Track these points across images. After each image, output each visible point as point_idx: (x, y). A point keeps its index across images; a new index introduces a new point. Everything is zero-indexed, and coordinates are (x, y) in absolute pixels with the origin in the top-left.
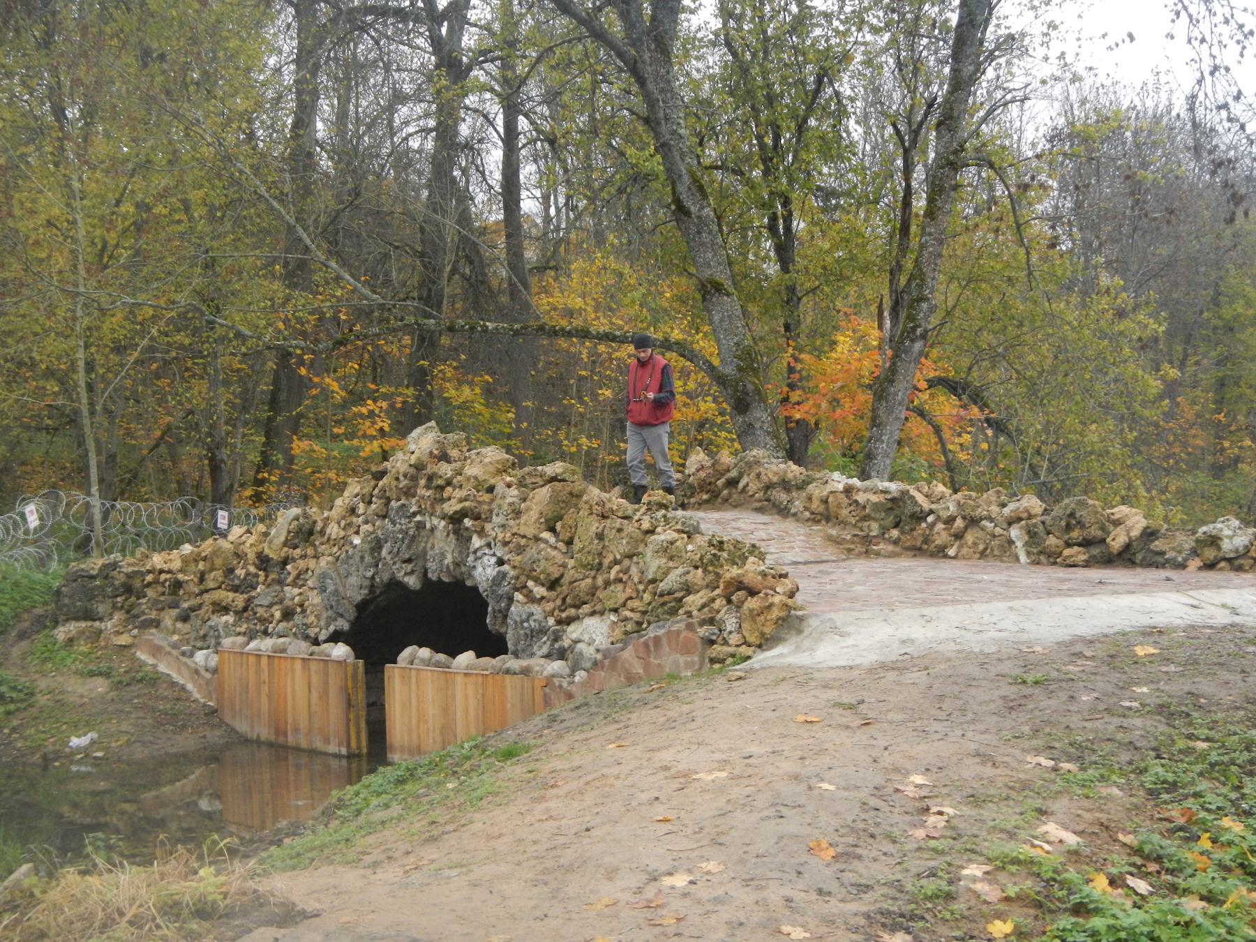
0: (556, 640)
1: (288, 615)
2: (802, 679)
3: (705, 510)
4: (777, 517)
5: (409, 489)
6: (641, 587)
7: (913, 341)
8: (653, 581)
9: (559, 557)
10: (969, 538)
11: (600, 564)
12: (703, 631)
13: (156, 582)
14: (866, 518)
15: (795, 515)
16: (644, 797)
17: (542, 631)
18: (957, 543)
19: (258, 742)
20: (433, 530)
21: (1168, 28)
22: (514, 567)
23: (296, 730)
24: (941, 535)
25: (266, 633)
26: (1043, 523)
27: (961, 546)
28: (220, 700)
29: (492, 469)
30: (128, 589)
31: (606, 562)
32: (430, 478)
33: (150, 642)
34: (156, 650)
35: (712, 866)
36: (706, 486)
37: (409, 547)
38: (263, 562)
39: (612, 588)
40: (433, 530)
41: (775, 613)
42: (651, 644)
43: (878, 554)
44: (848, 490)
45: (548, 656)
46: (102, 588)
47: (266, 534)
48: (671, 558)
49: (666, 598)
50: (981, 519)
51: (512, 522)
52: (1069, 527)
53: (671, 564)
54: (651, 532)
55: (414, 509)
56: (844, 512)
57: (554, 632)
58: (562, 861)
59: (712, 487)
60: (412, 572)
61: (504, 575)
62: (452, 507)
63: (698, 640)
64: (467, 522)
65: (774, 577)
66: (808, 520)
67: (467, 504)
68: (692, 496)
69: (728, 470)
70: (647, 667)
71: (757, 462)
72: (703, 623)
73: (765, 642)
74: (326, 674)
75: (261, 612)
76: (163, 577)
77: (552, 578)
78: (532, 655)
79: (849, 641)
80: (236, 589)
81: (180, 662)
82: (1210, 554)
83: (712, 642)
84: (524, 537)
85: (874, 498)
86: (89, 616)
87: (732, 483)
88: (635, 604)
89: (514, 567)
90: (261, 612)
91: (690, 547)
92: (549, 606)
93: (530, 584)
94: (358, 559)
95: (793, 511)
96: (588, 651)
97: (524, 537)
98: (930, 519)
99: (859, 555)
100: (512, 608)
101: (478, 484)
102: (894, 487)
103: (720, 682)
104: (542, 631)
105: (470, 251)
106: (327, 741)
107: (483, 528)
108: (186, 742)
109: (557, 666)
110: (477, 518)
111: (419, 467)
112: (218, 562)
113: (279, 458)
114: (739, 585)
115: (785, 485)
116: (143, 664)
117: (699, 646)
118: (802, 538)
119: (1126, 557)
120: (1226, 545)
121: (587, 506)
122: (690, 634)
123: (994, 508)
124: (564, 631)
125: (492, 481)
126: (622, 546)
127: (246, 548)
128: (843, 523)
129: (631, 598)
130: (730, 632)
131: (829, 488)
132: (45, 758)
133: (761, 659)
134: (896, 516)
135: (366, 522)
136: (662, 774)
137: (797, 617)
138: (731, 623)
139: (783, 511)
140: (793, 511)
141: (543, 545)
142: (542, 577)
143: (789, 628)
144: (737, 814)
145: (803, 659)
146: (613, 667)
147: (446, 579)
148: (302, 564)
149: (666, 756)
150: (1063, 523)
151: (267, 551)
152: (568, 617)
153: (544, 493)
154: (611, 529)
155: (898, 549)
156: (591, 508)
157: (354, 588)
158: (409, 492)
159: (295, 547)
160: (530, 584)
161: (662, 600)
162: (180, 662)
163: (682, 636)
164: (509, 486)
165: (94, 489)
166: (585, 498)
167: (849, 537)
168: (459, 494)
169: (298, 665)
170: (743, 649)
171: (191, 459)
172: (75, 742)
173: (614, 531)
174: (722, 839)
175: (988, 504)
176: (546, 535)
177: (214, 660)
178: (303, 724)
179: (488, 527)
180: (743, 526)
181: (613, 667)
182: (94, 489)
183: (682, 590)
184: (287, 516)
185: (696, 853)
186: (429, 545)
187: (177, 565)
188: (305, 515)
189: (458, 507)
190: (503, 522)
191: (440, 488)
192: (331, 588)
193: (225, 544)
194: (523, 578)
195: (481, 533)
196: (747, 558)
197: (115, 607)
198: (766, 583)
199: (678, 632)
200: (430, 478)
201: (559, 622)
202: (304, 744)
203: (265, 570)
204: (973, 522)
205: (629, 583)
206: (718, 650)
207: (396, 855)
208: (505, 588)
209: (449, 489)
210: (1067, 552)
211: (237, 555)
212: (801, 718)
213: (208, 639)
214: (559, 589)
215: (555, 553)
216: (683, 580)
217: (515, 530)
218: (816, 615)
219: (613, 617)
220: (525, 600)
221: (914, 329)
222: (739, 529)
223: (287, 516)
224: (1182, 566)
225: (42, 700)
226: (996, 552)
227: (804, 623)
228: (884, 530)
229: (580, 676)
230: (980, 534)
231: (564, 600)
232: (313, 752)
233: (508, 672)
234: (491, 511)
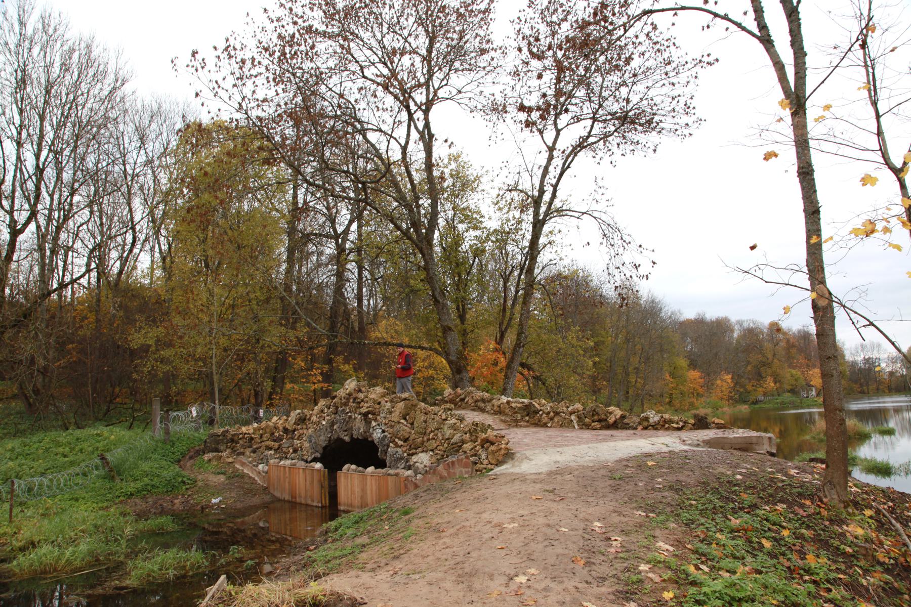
1: (295, 451)
2: (522, 478)
8: (448, 439)
10: (556, 420)
12: (472, 459)
13: (243, 438)
14: (516, 413)
16: (486, 536)
17: (402, 458)
19: (284, 501)
20: (355, 418)
21: (601, 240)
23: (300, 497)
24: (545, 418)
25: (286, 458)
28: (269, 484)
30: (232, 441)
31: (428, 432)
32: (355, 399)
33: (241, 461)
34: (243, 464)
35: (533, 571)
38: (286, 430)
40: (355, 418)
41: (503, 452)
43: (521, 426)
44: (508, 402)
45: (404, 468)
46: (222, 440)
47: (287, 420)
54: (446, 420)
58: (466, 571)
62: (364, 410)
64: (370, 416)
70: (449, 473)
72: (472, 456)
73: (499, 463)
74: (313, 474)
75: (284, 449)
78: (398, 468)
79: (533, 462)
80: (275, 441)
81: (253, 469)
82: (646, 424)
83: (476, 463)
85: (519, 405)
86: (217, 450)
87: (462, 400)
88: (441, 448)
90: (284, 449)
92: (405, 449)
96: (421, 466)
101: (375, 401)
102: (526, 401)
103: (486, 480)
104: (402, 458)
105: (347, 313)
106: (313, 501)
108: (256, 500)
109: (410, 472)
110: (374, 414)
111: (350, 394)
112: (268, 430)
113: (278, 390)
114: (486, 441)
115: (483, 400)
116: (238, 469)
119: (615, 426)
120: (651, 420)
123: (565, 408)
126: (435, 425)
127: (279, 425)
128: (507, 415)
131: (500, 402)
132: (202, 508)
133: (498, 470)
136: (489, 526)
138: (484, 456)
144: (532, 544)
145: (516, 470)
146: (434, 473)
148: (301, 431)
149: (486, 516)
157: (323, 441)
158: (346, 404)
162: (253, 469)
165: (217, 402)
169: (301, 471)
170: (489, 466)
171: (247, 389)
174: (533, 558)
175: (562, 407)
176: (402, 421)
177: (266, 468)
178: (303, 494)
181: (434, 473)
184: (294, 414)
185: (523, 565)
187: (251, 431)
188: (303, 413)
191: (359, 403)
193: (270, 424)
195: (376, 420)
197: (227, 447)
200: (355, 399)
202: (303, 502)
204: (557, 414)
206: (479, 466)
207: (382, 565)
211: (275, 428)
212: (534, 497)
213: (264, 460)
223: (294, 414)
224: (636, 429)
225: (200, 484)
228: (523, 417)
229: (419, 476)
232: (307, 505)
233: (389, 475)
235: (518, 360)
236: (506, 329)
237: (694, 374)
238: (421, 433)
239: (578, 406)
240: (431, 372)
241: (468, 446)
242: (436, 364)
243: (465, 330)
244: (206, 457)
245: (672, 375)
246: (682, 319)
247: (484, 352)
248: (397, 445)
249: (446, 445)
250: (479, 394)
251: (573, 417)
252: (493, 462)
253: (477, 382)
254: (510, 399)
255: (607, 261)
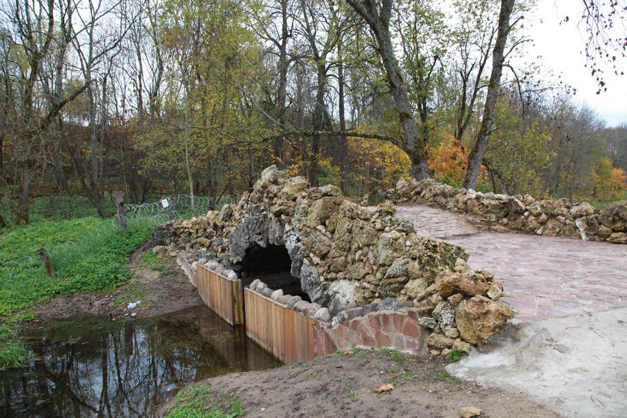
0: (325, 289)
3: (406, 206)
4: (440, 210)
5: (260, 198)
6: (375, 268)
7: (485, 136)
8: (383, 265)
9: (327, 241)
10: (550, 225)
11: (350, 248)
15: (449, 209)
17: (318, 284)
18: (542, 227)
22: (304, 244)
24: (532, 222)
26: (596, 218)
27: (544, 229)
29: (296, 188)
30: (175, 234)
31: (354, 247)
36: (405, 194)
37: (259, 227)
38: (215, 226)
39: (357, 265)
41: (492, 321)
42: (381, 319)
43: (496, 231)
44: (478, 198)
48: (395, 250)
49: (392, 280)
50: (558, 215)
51: (303, 218)
52: (614, 221)
53: (395, 254)
54: (382, 230)
55: (262, 208)
56: (476, 209)
57: (323, 285)
59: (408, 195)
60: (262, 239)
61: (298, 248)
62: (276, 208)
63: (418, 327)
64: (283, 217)
65: (483, 281)
66: (456, 212)
67: (282, 207)
68: (399, 198)
69: (416, 188)
70: (378, 334)
71: (430, 184)
72: (422, 314)
73: (481, 345)
76: (186, 230)
77: (323, 254)
80: (207, 237)
83: (430, 331)
84: (309, 227)
85: (493, 202)
86: (162, 243)
87: (418, 193)
89: (304, 244)
91: (408, 243)
92: (321, 270)
93: (311, 255)
94: (242, 230)
95: (448, 207)
97: (309, 227)
98: (526, 214)
99: (485, 230)
100: (302, 268)
102: (504, 197)
107: (290, 220)
112: (202, 225)
115: (444, 195)
117: (419, 332)
118: (455, 221)
121: (342, 212)
122: (412, 321)
123: (565, 210)
124: (329, 285)
125: (296, 195)
128: (475, 214)
129: (368, 274)
130: (446, 325)
134: (505, 212)
135: (247, 213)
137: (513, 326)
138: (446, 318)
139: (443, 207)
140: (448, 207)
141: (318, 233)
142: (317, 252)
143: (506, 336)
147: (276, 244)
150: (611, 219)
151: (217, 223)
152: (331, 278)
153: (320, 202)
154: (357, 227)
155: (507, 229)
156: (345, 213)
159: (226, 221)
160: (311, 255)
161: (389, 281)
163: (406, 320)
164: (304, 198)
165: (192, 193)
166: (341, 206)
167: (479, 221)
168: (279, 201)
170: (458, 343)
172: (131, 305)
173: (358, 229)
176: (320, 227)
179: (293, 220)
180: (426, 215)
182: (192, 193)
183: (403, 275)
186: (270, 226)
187: (190, 226)
189: (278, 209)
190: (299, 218)
192: (234, 242)
194: (307, 251)
195: (290, 222)
196: (455, 259)
198: (477, 287)
199: (402, 317)
201: (326, 279)
203: (216, 230)
204: (552, 216)
205: (367, 264)
208: (299, 256)
209: (276, 199)
210: (614, 235)
214: (327, 260)
215: (324, 238)
216: (404, 268)
217: (304, 223)
218: (529, 324)
219: (357, 284)
220: (309, 264)
221: (486, 130)
222: (424, 217)
226: (567, 233)
227: (520, 332)
228: (498, 219)
230: (557, 223)
231: (329, 267)
234: (294, 211)
235: (480, 155)
236: (465, 125)
237: (618, 172)
238: (343, 249)
239: (587, 207)
240: (397, 166)
241: (416, 287)
242: (401, 160)
243: (426, 128)
244: (155, 249)
245: (598, 172)
246: (607, 126)
247: (444, 147)
248: (312, 263)
249: (379, 275)
250: (439, 187)
251: (578, 223)
252: (467, 336)
253: (436, 176)
254: (480, 193)
255: (587, 40)
